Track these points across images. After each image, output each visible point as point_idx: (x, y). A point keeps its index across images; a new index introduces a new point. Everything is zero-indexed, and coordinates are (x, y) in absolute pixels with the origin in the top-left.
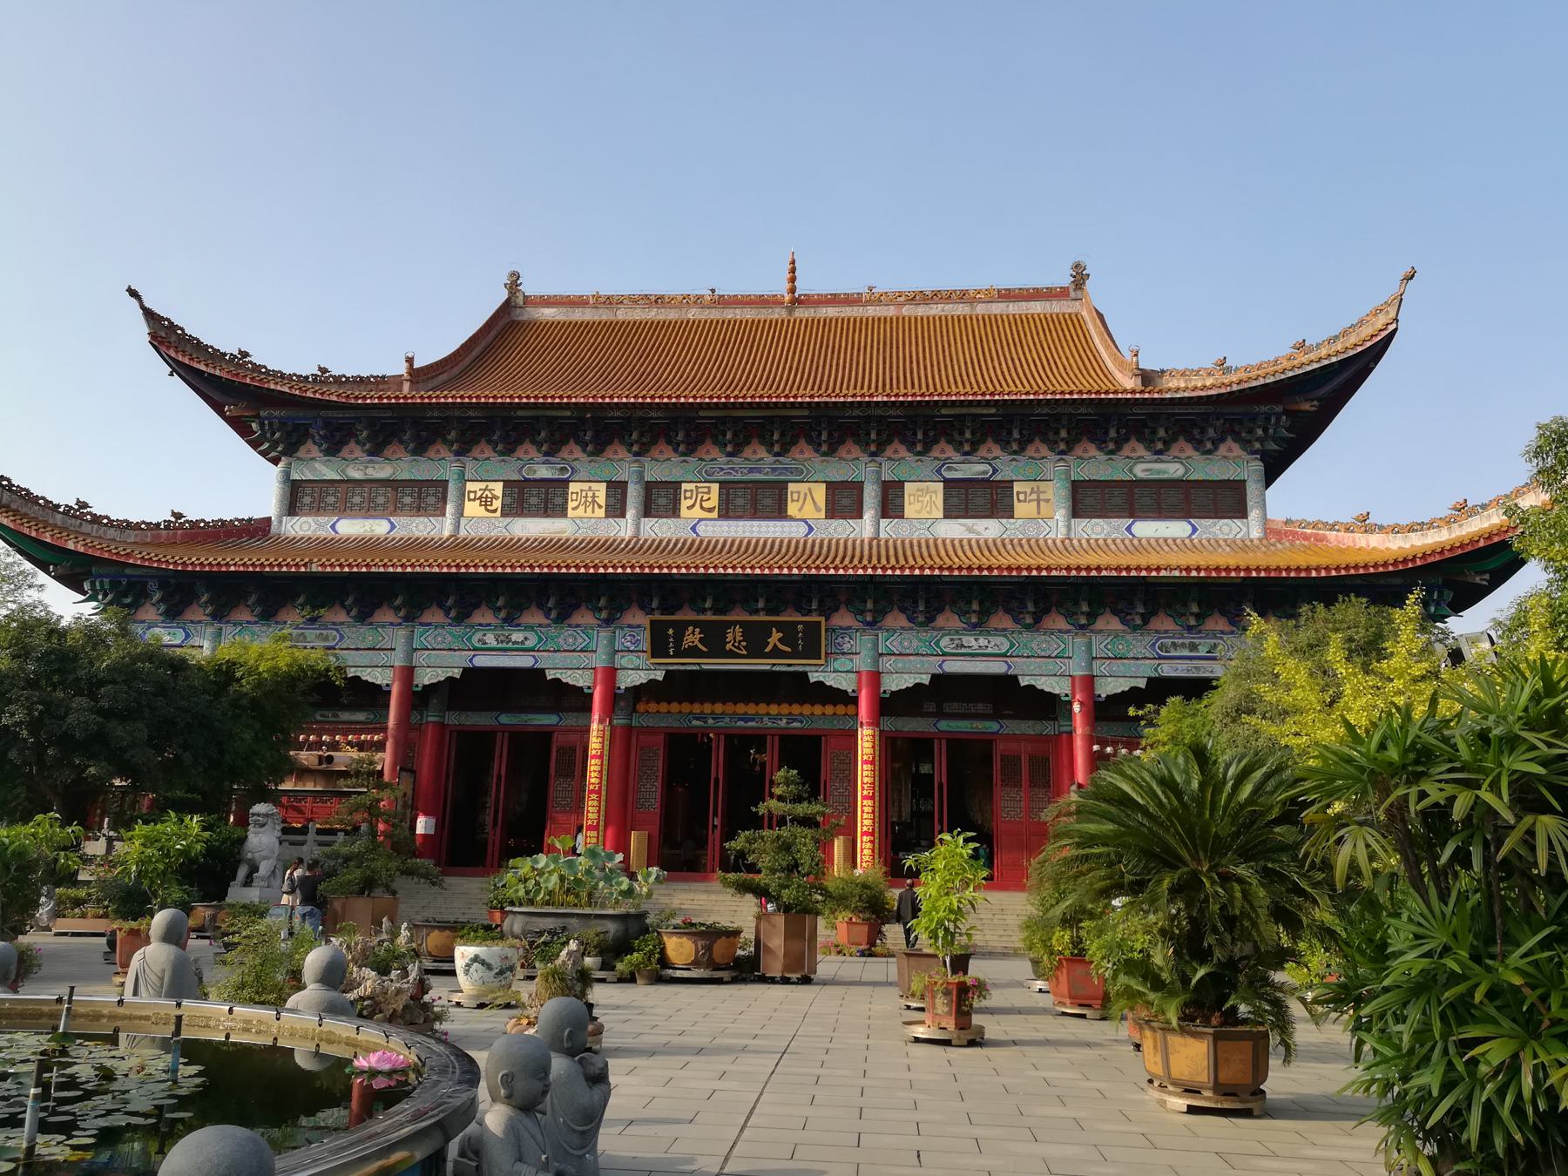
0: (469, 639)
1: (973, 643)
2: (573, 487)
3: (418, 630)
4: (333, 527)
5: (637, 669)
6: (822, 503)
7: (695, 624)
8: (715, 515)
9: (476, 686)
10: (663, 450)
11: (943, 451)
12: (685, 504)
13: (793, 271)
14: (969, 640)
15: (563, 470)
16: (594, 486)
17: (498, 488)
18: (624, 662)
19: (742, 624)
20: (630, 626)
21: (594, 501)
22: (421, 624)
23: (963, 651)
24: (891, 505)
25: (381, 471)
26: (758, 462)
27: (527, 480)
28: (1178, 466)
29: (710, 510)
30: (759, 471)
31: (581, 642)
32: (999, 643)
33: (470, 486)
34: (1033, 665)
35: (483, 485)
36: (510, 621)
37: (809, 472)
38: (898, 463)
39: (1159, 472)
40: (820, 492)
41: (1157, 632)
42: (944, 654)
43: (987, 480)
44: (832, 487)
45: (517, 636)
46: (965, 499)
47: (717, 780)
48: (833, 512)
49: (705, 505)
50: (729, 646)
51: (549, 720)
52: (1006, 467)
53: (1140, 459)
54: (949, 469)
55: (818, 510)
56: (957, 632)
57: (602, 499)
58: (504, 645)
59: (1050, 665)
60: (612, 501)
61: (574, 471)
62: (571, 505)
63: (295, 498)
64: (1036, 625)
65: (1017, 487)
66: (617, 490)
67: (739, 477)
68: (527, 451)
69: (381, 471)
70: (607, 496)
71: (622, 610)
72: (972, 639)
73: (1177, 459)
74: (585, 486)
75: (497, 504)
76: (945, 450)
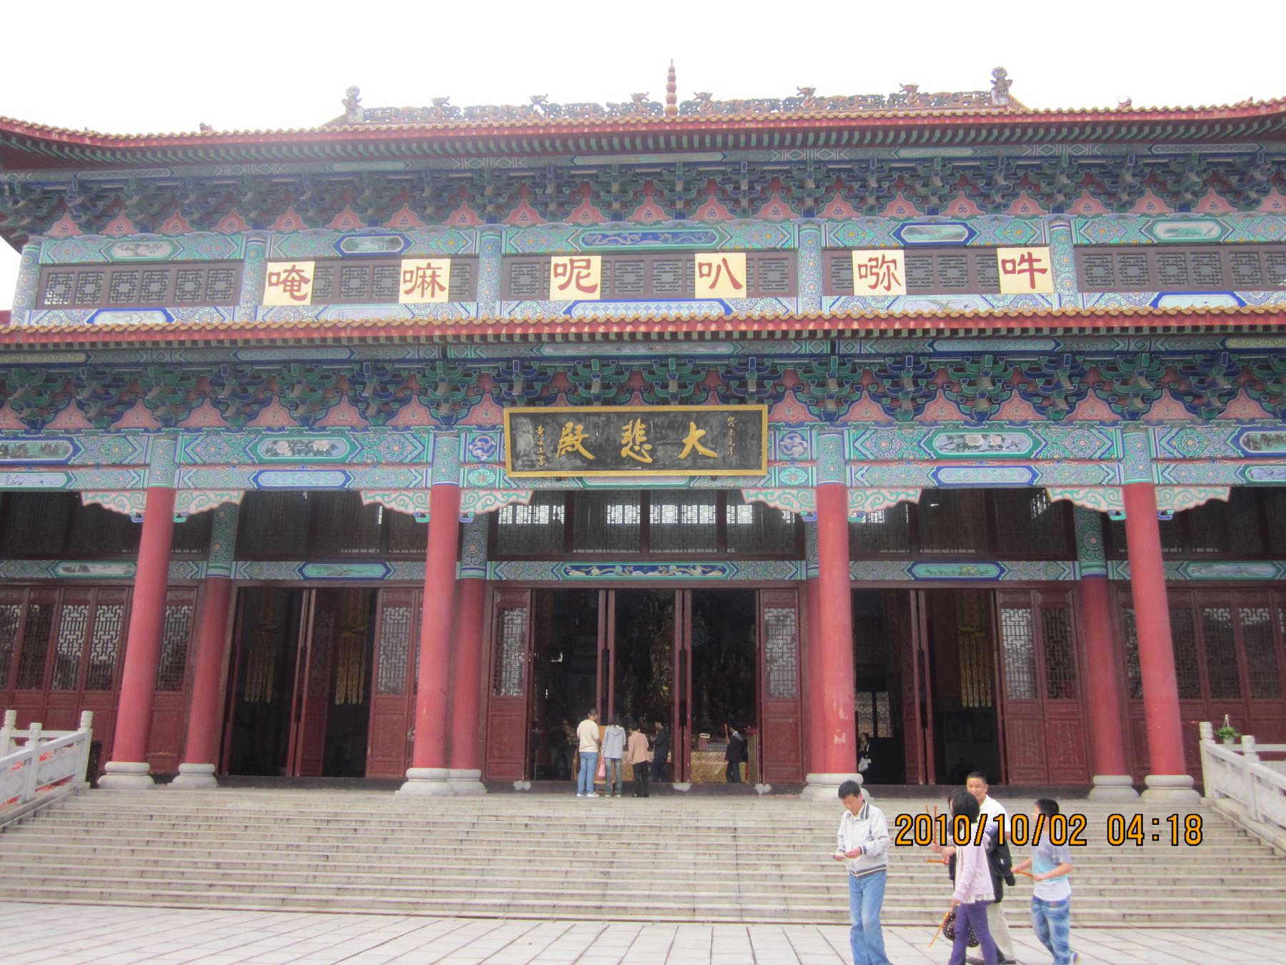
0: (254, 449)
1: (981, 442)
2: (407, 265)
3: (184, 438)
4: (300, 570)
5: (491, 488)
6: (742, 278)
7: (577, 418)
8: (596, 295)
9: (270, 523)
10: (524, 213)
11: (900, 210)
12: (555, 282)
13: (672, 79)
14: (976, 438)
15: (394, 242)
16: (435, 263)
17: (308, 269)
18: (473, 478)
19: (646, 417)
20: (480, 427)
21: (434, 281)
22: (187, 430)
23: (967, 453)
24: (837, 275)
25: (157, 250)
26: (650, 224)
27: (345, 257)
28: (1211, 225)
29: (591, 289)
30: (656, 237)
31: (410, 452)
32: (1019, 442)
33: (272, 267)
34: (1065, 472)
35: (289, 266)
36: (308, 422)
37: (723, 237)
38: (839, 224)
39: (1187, 232)
40: (738, 262)
41: (1239, 421)
42: (939, 459)
43: (963, 246)
44: (753, 256)
45: (321, 444)
46: (684, 569)
47: (606, 652)
48: (758, 286)
49: (583, 282)
50: (625, 452)
51: (374, 571)
52: (987, 228)
53: (1160, 217)
54: (911, 232)
55: (737, 285)
56: (957, 428)
57: (444, 279)
58: (302, 457)
59: (1093, 472)
60: (458, 281)
61: (408, 243)
62: (404, 287)
63: (43, 281)
64: (1063, 418)
65: (1002, 254)
66: (464, 267)
67: (628, 246)
68: (347, 220)
69: (157, 250)
70: (452, 275)
71: (467, 404)
72: (979, 436)
73: (1209, 217)
74: (423, 263)
75: (307, 289)
76: (901, 207)
